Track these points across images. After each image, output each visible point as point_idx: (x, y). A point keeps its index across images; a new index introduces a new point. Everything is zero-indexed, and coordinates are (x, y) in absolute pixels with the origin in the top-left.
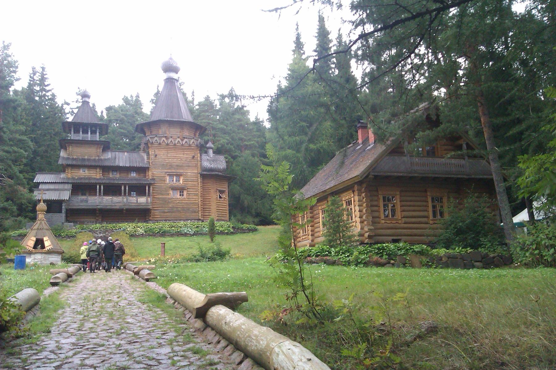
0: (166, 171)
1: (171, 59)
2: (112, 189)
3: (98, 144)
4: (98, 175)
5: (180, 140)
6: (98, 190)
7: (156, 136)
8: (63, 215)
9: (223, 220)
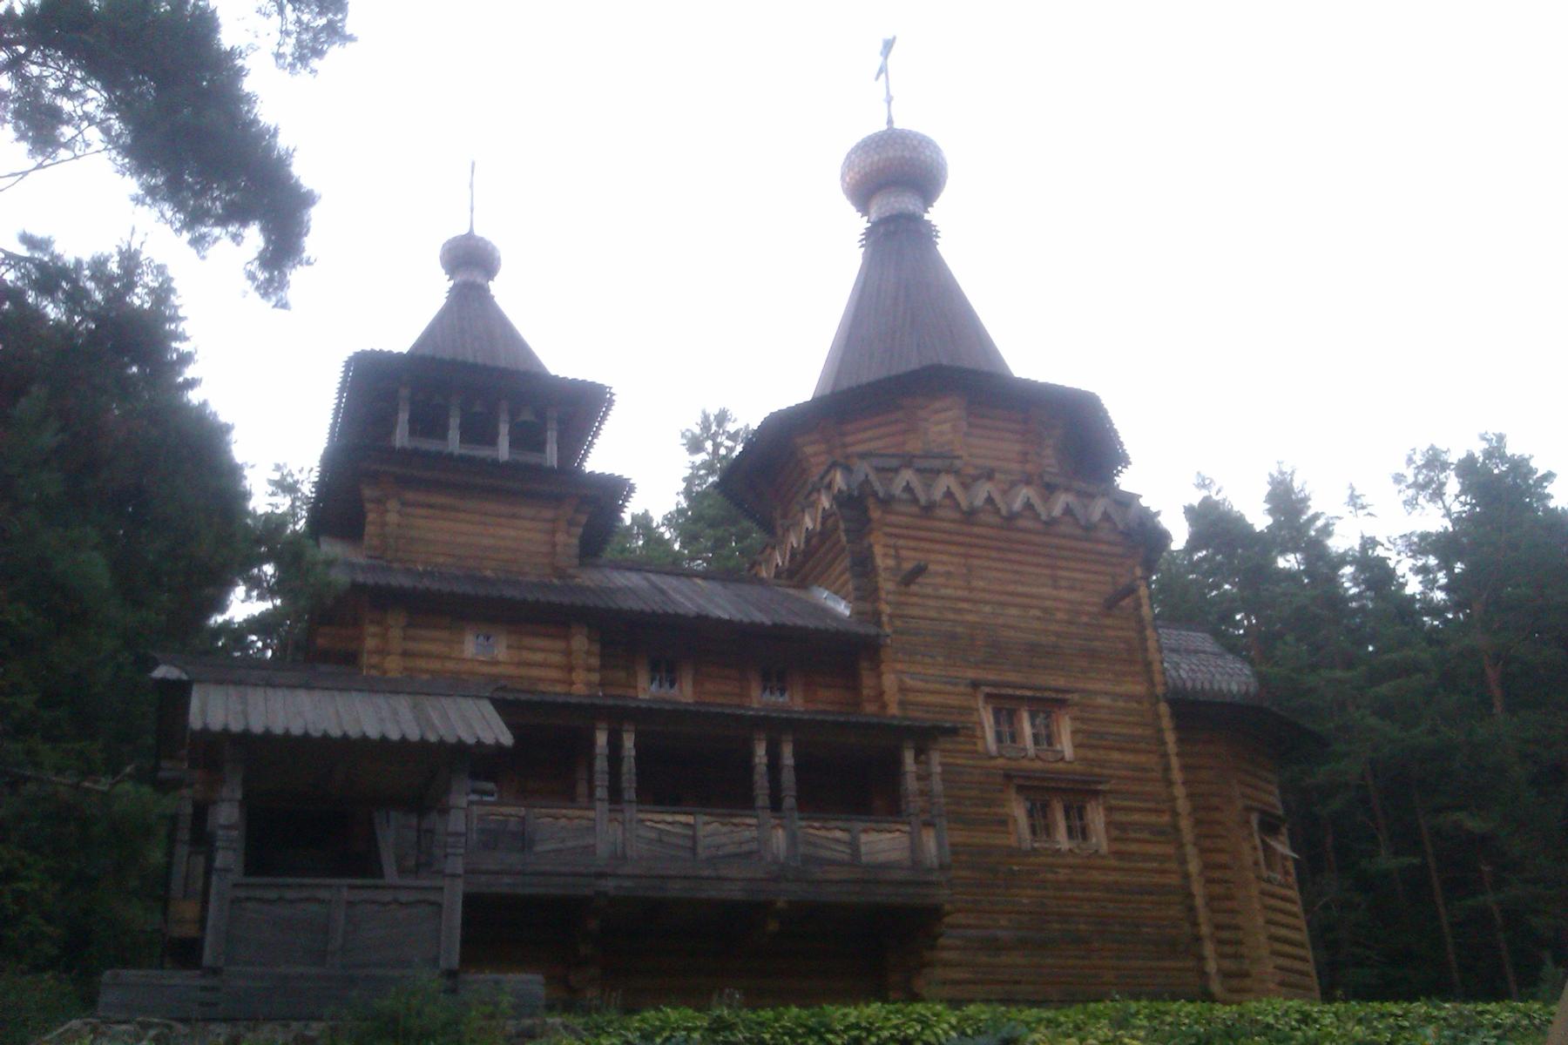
0: (971, 674)
4: (579, 676)
6: (601, 764)
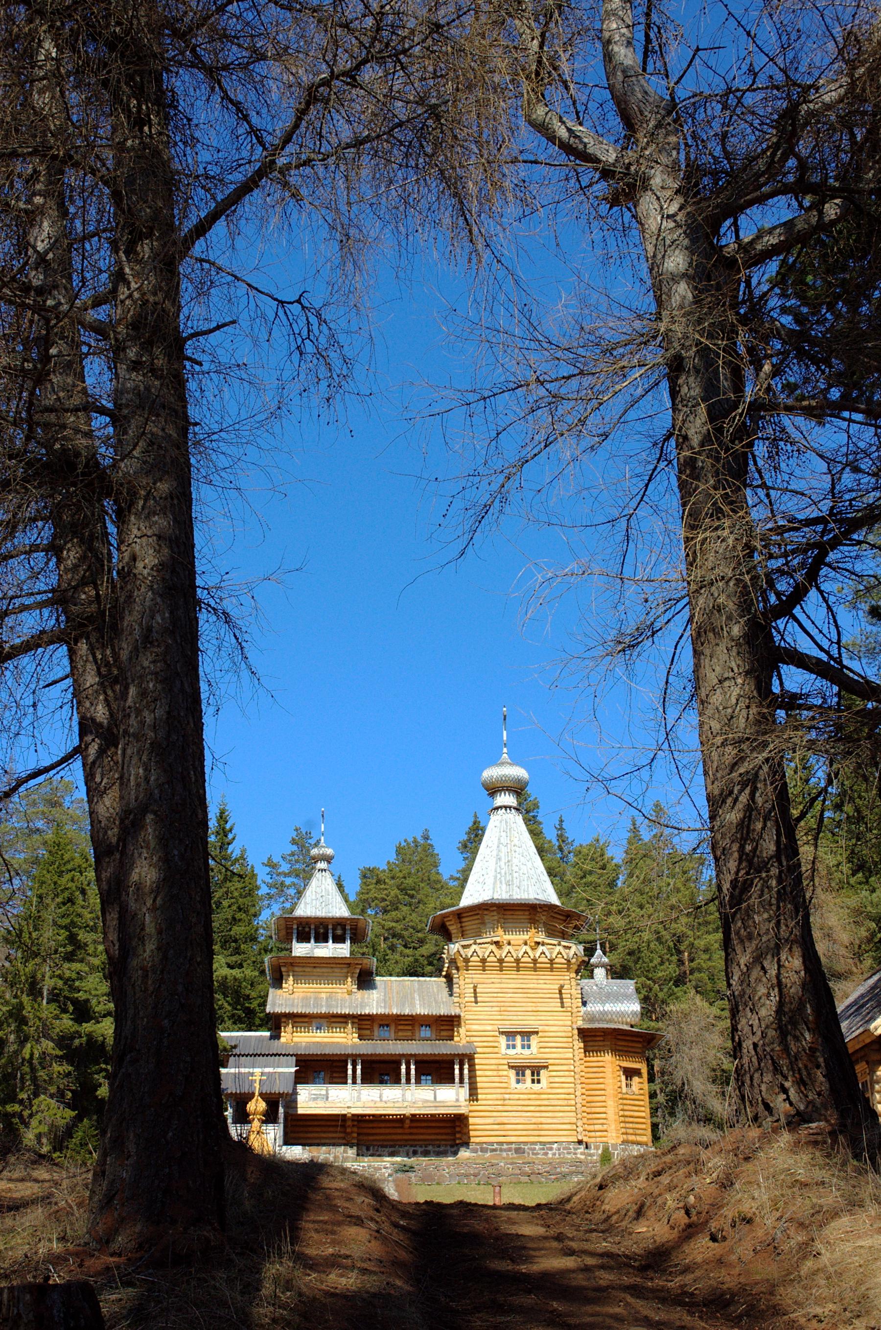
2: (380, 1071)
7: (475, 943)
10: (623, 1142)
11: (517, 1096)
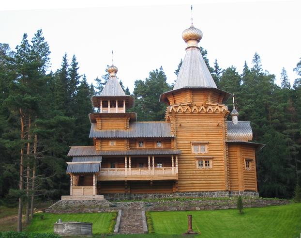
1: (192, 28)
2: (139, 161)
3: (125, 116)
5: (204, 108)
8: (94, 187)
9: (251, 191)
10: (245, 191)
11: (199, 172)
